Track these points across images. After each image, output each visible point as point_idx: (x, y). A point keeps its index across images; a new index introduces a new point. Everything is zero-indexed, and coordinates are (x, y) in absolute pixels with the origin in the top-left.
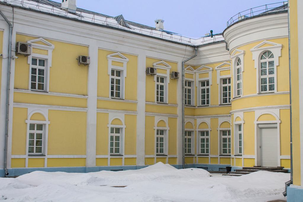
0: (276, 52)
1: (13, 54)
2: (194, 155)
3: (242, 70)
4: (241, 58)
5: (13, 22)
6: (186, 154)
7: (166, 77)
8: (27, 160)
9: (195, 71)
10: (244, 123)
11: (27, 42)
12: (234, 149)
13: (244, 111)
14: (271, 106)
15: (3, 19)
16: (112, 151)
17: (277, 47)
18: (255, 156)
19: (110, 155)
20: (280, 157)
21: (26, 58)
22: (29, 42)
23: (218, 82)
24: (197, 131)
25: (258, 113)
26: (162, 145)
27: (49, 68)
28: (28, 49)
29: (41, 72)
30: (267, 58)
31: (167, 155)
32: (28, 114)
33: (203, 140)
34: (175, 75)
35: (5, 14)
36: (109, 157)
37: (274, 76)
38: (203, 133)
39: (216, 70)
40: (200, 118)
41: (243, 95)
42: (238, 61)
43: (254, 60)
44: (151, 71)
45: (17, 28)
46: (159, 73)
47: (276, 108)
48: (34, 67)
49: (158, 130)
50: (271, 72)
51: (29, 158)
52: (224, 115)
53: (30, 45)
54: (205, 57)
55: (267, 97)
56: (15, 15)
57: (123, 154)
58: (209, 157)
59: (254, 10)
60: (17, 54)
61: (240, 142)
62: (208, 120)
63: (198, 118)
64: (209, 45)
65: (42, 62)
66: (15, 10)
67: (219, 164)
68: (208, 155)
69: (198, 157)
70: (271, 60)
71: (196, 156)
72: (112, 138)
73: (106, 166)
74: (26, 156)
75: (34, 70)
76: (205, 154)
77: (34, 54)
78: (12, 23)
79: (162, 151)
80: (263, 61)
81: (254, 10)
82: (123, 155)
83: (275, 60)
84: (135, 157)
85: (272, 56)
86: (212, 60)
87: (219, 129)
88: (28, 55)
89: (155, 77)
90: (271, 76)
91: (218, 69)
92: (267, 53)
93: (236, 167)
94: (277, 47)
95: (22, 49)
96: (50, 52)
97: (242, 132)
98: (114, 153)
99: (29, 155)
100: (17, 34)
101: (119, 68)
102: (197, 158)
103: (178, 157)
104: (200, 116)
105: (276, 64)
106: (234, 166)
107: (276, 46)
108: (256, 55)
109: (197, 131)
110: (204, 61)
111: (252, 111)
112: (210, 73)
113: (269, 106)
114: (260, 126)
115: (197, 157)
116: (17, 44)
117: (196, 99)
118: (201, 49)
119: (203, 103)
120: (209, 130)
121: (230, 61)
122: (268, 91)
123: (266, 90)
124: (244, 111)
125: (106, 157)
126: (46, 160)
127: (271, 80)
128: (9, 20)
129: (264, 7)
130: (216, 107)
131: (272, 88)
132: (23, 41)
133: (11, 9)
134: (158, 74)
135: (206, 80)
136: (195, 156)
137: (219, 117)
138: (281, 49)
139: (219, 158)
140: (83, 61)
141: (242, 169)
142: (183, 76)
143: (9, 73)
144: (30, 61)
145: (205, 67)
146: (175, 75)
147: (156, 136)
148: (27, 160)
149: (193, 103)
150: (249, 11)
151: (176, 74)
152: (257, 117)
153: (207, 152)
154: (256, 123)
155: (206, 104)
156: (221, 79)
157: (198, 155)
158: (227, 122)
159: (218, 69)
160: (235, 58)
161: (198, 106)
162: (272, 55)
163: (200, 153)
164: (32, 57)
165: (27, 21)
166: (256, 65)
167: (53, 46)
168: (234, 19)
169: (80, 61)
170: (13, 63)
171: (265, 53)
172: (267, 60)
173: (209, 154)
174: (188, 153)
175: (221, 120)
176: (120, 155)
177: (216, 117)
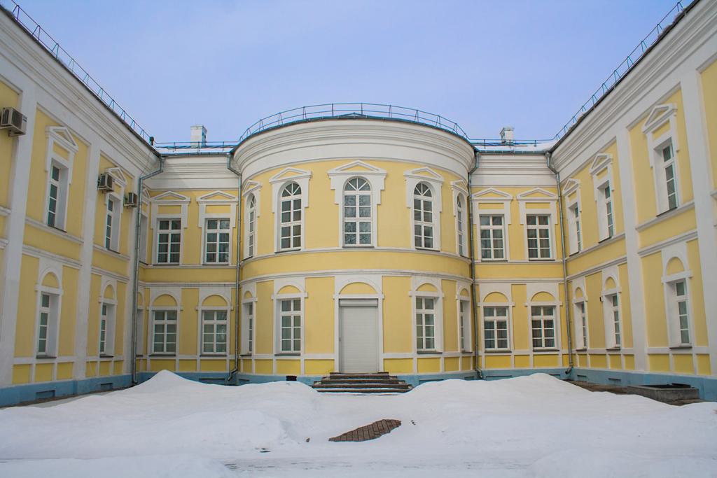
0: (376, 183)
2: (142, 356)
9: (150, 200)
12: (57, 347)
13: (307, 276)
14: (368, 270)
16: (419, 345)
17: (380, 174)
19: (101, 357)
20: (382, 356)
23: (202, 223)
24: (150, 312)
25: (340, 281)
26: (429, 331)
30: (292, 195)
31: (141, 354)
33: (209, 328)
36: (34, 361)
39: (517, 200)
40: (158, 286)
41: (305, 248)
44: (105, 183)
47: (375, 273)
50: (365, 213)
51: (418, 359)
52: (214, 283)
54: (174, 177)
55: (357, 257)
58: (302, 358)
59: (307, 110)
61: (103, 333)
62: (176, 292)
63: (152, 286)
64: (188, 157)
67: (198, 371)
68: (299, 355)
69: (674, 355)
70: (297, 197)
72: (419, 317)
73: (28, 384)
76: (292, 351)
82: (55, 358)
83: (375, 195)
85: (367, 188)
86: (190, 184)
87: (200, 308)
91: (202, 200)
92: (357, 182)
94: (380, 174)
97: (101, 317)
98: (425, 349)
102: (149, 361)
103: (125, 359)
104: (156, 283)
105: (375, 199)
106: (251, 371)
107: (377, 172)
108: (339, 182)
109: (150, 312)
110: (172, 184)
111: (330, 276)
112: (185, 206)
113: (365, 270)
114: (342, 302)
115: (149, 358)
118: (169, 161)
120: (178, 308)
122: (292, 247)
123: (353, 242)
124: (587, 274)
125: (409, 355)
130: (194, 268)
131: (298, 242)
135: (537, 215)
136: (144, 358)
137: (203, 286)
138: (385, 179)
139: (198, 362)
145: (173, 195)
147: (413, 311)
150: (414, 113)
152: (338, 288)
154: (337, 297)
156: (206, 219)
157: (150, 356)
158: (222, 297)
159: (202, 200)
160: (283, 183)
161: (153, 264)
162: (367, 185)
163: (281, 351)
168: (265, 122)
171: (353, 181)
172: (357, 193)
173: (302, 352)
174: (167, 351)
175: (204, 293)
177: (194, 286)
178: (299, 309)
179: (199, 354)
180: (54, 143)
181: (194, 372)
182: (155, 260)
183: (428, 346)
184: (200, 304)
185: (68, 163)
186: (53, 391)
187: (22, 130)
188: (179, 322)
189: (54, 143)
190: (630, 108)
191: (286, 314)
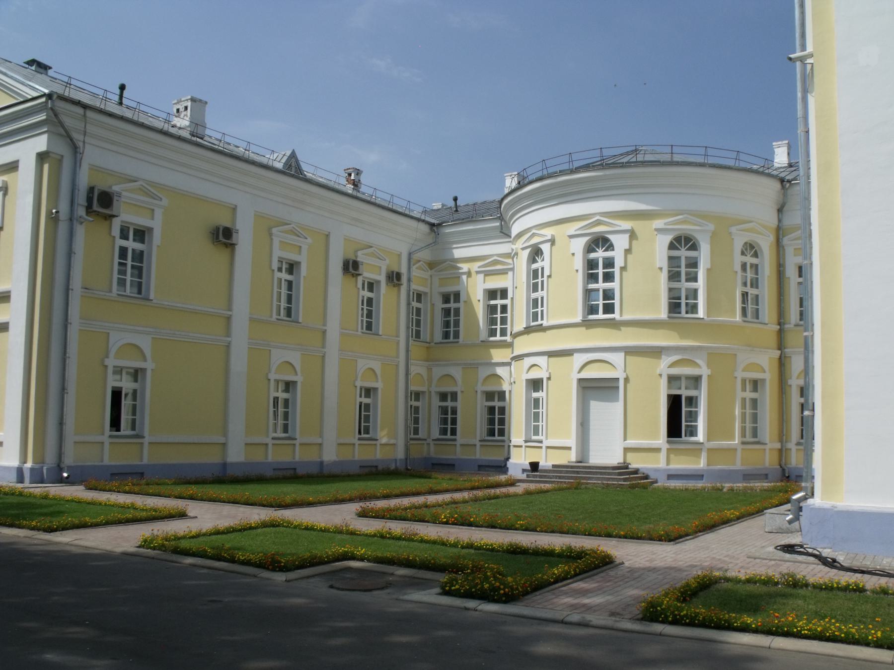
0: (620, 242)
1: (81, 212)
3: (546, 273)
4: (545, 248)
5: (84, 142)
6: (275, 435)
7: (379, 282)
8: (107, 446)
10: (549, 379)
11: (110, 187)
15: (63, 132)
18: (571, 441)
21: (107, 222)
22: (116, 188)
24: (433, 394)
27: (155, 249)
28: (115, 203)
29: (139, 256)
32: (110, 346)
34: (394, 278)
35: (68, 122)
37: (615, 285)
38: (443, 396)
42: (536, 253)
43: (573, 254)
44: (351, 267)
45: (92, 156)
46: (368, 274)
48: (124, 243)
49: (744, 381)
50: (608, 277)
53: (119, 195)
56: (88, 126)
57: (767, 441)
59: (549, 163)
60: (89, 208)
62: (457, 372)
65: (141, 234)
66: (90, 114)
68: (455, 440)
71: (429, 441)
74: (105, 439)
75: (123, 252)
77: (127, 214)
78: (81, 144)
79: (416, 431)
80: (593, 255)
81: (549, 163)
84: (470, 443)
85: (610, 247)
86: (458, 253)
88: (114, 216)
89: (360, 279)
90: (608, 285)
93: (483, 458)
95: (101, 202)
96: (159, 213)
98: (363, 436)
99: (110, 436)
100: (94, 168)
101: (294, 257)
105: (619, 263)
108: (579, 245)
115: (432, 443)
116: (91, 190)
117: (433, 327)
119: (446, 335)
120: (458, 389)
121: (513, 255)
126: (146, 446)
127: (608, 295)
128: (75, 136)
129: (597, 153)
132: (102, 184)
133: (80, 111)
134: (366, 274)
140: (224, 236)
141: (551, 468)
142: (409, 280)
143: (70, 253)
144: (116, 232)
146: (394, 278)
148: (107, 446)
149: (425, 335)
151: (398, 276)
153: (454, 432)
154: (576, 376)
155: (452, 339)
156: (485, 290)
164: (122, 222)
165: (113, 143)
166: (578, 263)
167: (165, 202)
169: (217, 237)
170: (80, 231)
176: (758, 443)
178: (456, 401)
179: (478, 438)
180: (280, 242)
181: (732, 468)
182: (438, 337)
183: (755, 434)
184: (479, 384)
185: (303, 259)
186: (295, 469)
187: (234, 242)
188: (459, 405)
189: (280, 242)
190: (693, 194)
191: (444, 404)
